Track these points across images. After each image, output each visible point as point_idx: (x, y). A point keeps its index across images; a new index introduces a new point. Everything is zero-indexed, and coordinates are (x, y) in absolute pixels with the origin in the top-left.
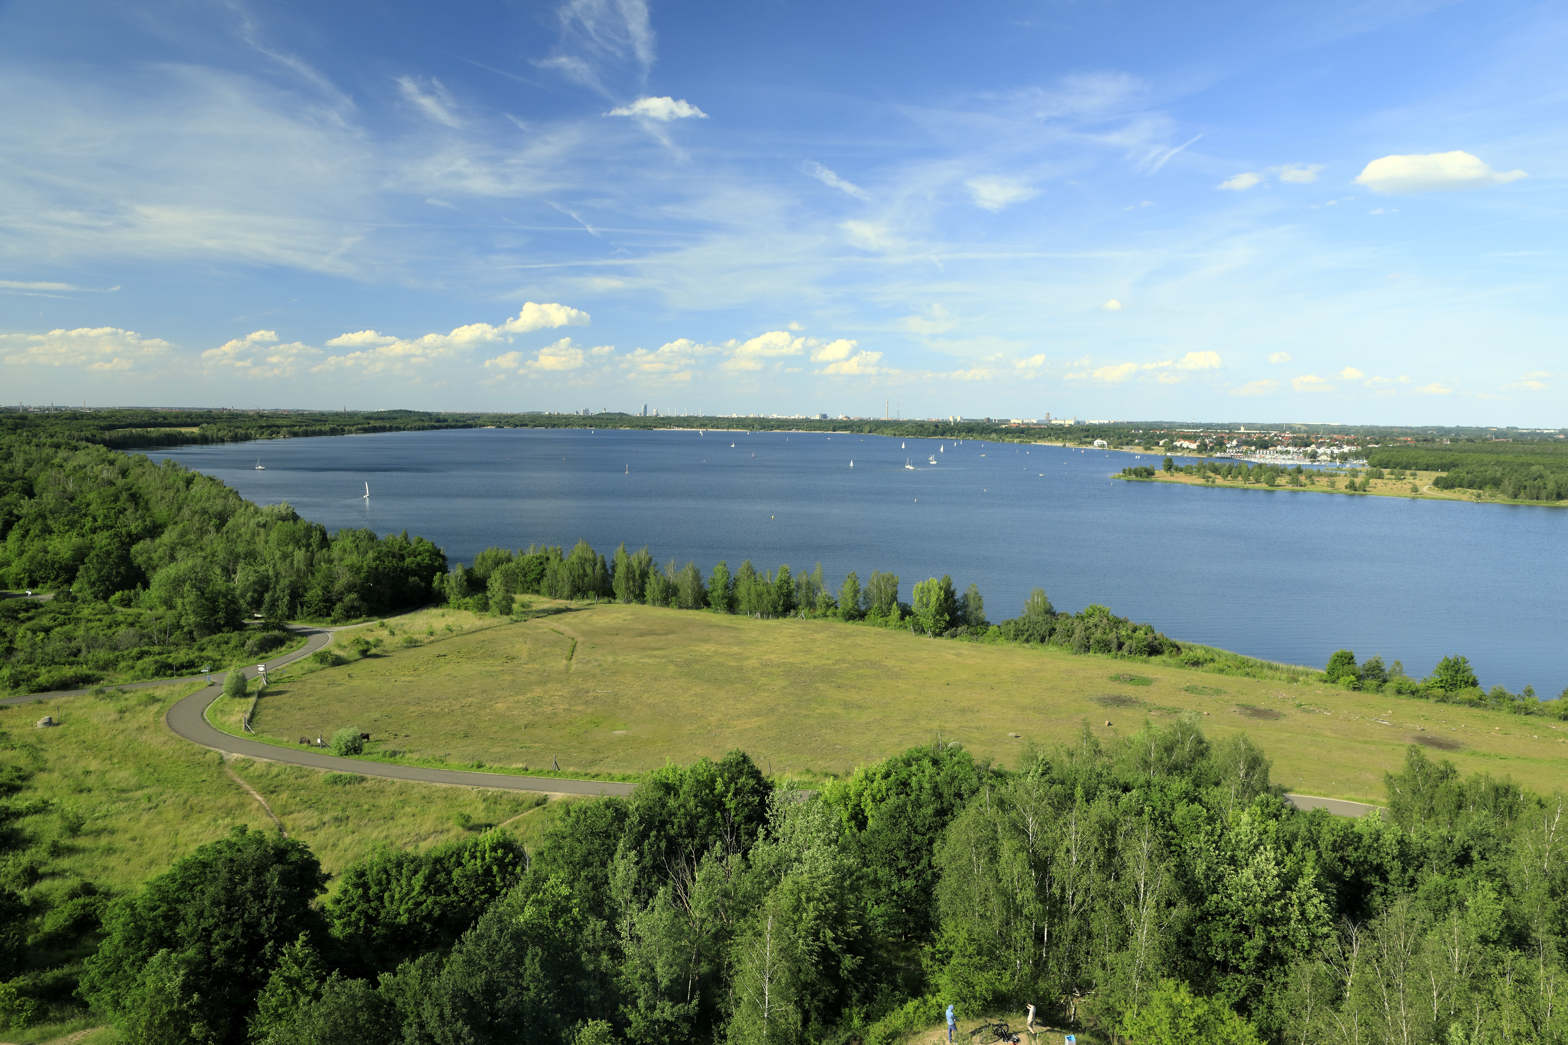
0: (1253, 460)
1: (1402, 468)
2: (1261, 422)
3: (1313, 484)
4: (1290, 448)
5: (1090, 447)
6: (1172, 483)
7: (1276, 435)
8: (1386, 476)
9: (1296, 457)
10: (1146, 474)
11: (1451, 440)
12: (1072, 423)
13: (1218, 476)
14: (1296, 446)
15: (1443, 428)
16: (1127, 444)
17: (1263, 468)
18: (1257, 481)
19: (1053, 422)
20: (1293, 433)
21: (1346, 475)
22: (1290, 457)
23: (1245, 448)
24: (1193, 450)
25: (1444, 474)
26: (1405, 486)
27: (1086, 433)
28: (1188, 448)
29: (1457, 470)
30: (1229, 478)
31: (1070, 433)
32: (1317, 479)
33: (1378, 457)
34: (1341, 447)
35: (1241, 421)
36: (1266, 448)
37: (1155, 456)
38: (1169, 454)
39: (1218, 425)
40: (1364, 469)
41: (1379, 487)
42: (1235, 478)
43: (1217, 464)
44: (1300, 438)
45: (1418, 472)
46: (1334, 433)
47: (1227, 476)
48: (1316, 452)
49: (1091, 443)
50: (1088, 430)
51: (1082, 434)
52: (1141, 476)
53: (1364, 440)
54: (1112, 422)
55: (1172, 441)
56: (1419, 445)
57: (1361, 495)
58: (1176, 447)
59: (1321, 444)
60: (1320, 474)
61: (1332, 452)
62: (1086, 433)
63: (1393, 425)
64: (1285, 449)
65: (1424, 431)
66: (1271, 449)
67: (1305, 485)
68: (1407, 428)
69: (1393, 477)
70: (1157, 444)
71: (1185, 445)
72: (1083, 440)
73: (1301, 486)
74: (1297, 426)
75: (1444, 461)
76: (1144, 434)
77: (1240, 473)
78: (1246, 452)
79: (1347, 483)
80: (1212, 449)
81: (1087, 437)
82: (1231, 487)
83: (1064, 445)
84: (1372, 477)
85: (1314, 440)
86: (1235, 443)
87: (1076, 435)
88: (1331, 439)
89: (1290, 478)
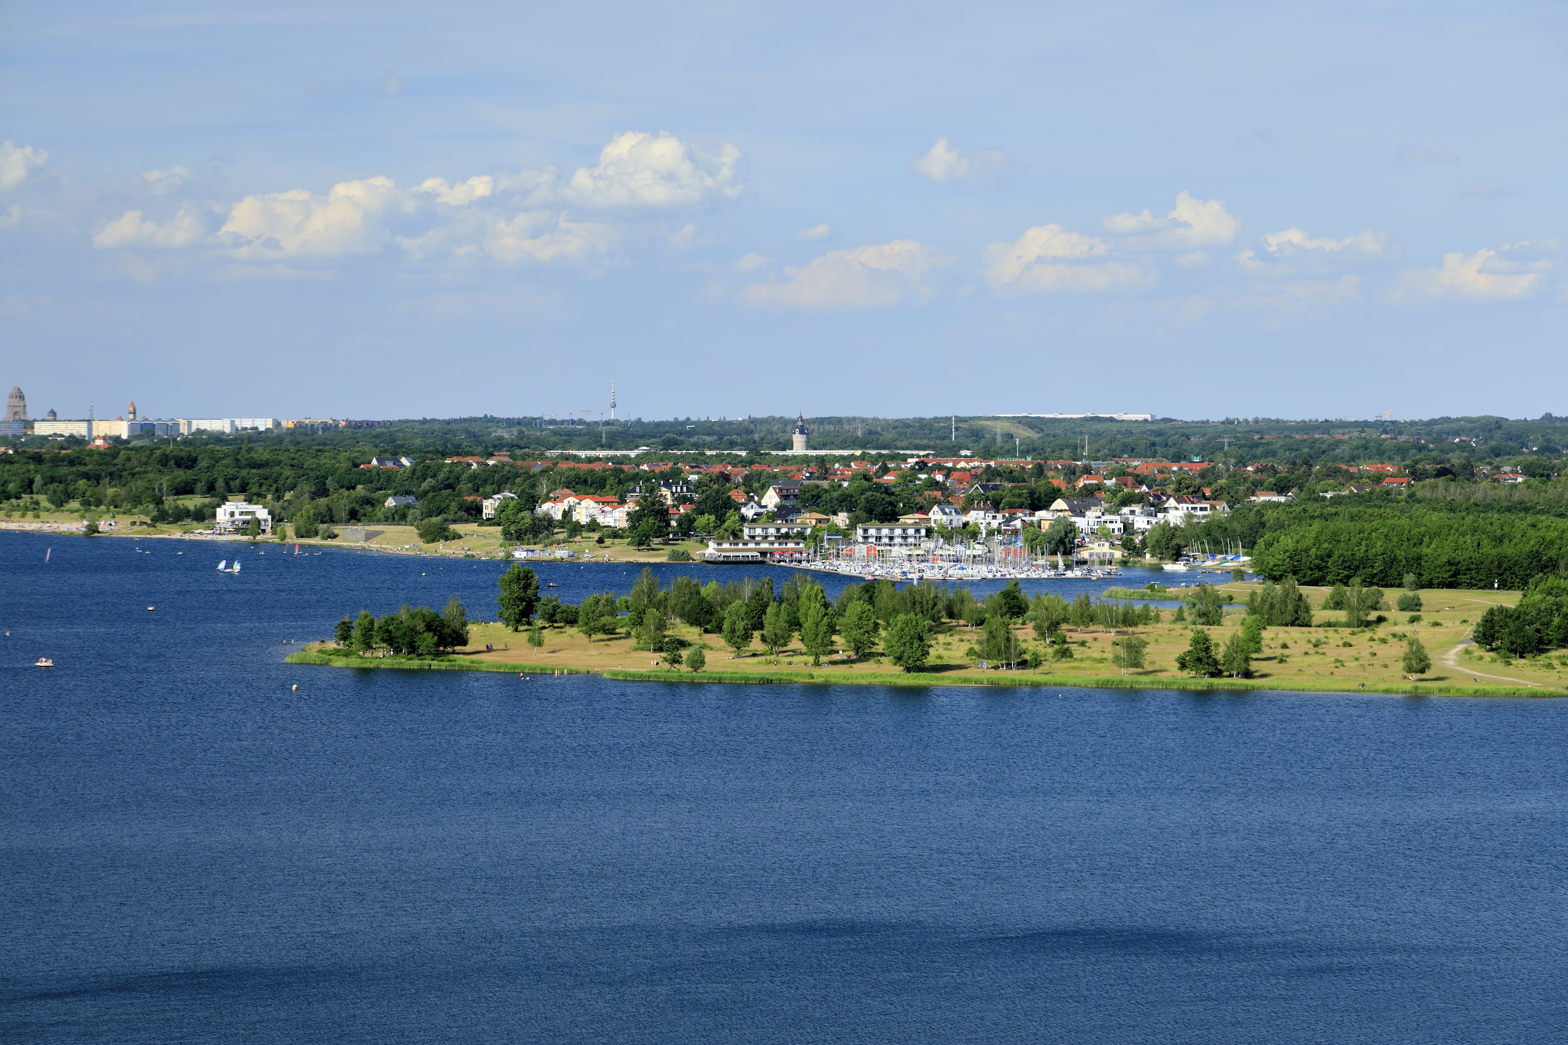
0: (844, 567)
1: (1368, 582)
2: (868, 413)
3: (1065, 654)
4: (976, 517)
5: (200, 533)
6: (539, 675)
7: (922, 466)
8: (1319, 615)
9: (999, 552)
10: (430, 638)
11: (1529, 471)
12: (122, 430)
13: (714, 639)
14: (996, 506)
15: (1498, 423)
16: (354, 516)
17: (884, 598)
18: (863, 654)
19: (42, 429)
20: (987, 454)
21: (1180, 618)
22: (979, 550)
23: (808, 520)
24: (616, 534)
25: (1510, 600)
26: (1383, 651)
27: (181, 475)
28: (593, 526)
29: (1552, 581)
30: (756, 644)
31: (115, 477)
32: (1077, 636)
33: (1287, 542)
34: (1158, 507)
35: (792, 414)
36: (890, 516)
37: (469, 565)
38: (520, 554)
39: (707, 428)
40: (1241, 590)
41: (1296, 660)
42: (777, 642)
43: (709, 590)
44: (1010, 476)
45: (1425, 595)
46: (1133, 452)
47: (747, 637)
48: (1071, 529)
49: (203, 516)
50: (189, 462)
51: (165, 481)
52: (413, 649)
53: (1237, 478)
54: (288, 424)
55: (531, 501)
56: (1421, 490)
57: (1238, 695)
58: (548, 523)
59: (1089, 495)
60: (1088, 618)
61: (1127, 527)
62: (181, 475)
63: (1333, 416)
64: (959, 520)
65: (1439, 438)
66: (908, 519)
67: (1037, 663)
68: (1381, 426)
69: (1341, 615)
70: (474, 512)
71: (581, 516)
72: (170, 502)
73: (1023, 664)
74: (1000, 428)
75: (1508, 549)
76: (420, 473)
77: (795, 624)
78: (815, 538)
79: (1186, 646)
80: (687, 529)
81: (186, 489)
82: (766, 683)
83: (93, 529)
84: (1270, 622)
85: (1059, 482)
86: (771, 499)
87: (139, 484)
88: (1121, 474)
89: (981, 634)
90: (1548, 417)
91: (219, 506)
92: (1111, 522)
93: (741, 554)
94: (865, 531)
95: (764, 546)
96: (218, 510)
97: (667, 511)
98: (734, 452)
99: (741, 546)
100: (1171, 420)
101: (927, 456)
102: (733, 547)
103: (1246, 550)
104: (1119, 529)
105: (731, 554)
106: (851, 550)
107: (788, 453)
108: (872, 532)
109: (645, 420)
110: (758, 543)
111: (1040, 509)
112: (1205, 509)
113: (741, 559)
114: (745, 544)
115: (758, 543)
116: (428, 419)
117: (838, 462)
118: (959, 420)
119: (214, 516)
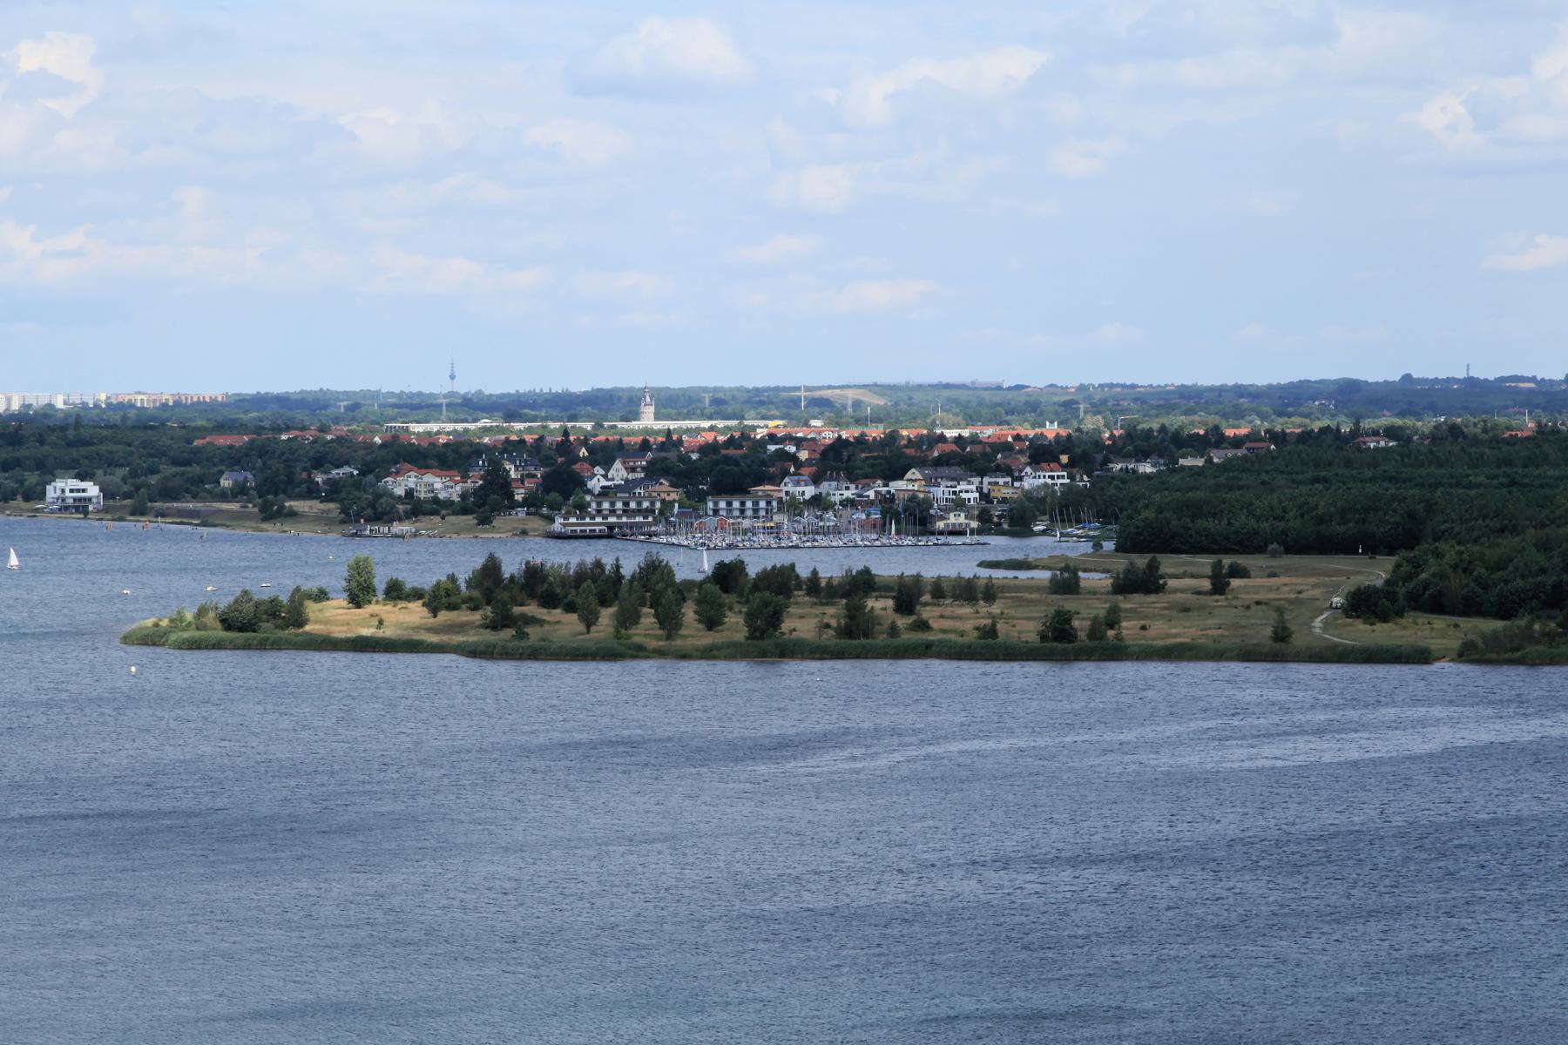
20: (838, 423)
91: (49, 483)
92: (967, 492)
94: (716, 504)
95: (612, 520)
97: (510, 483)
98: (578, 424)
99: (588, 520)
100: (1023, 387)
101: (777, 427)
103: (699, 405)
104: (975, 499)
108: (736, 504)
110: (605, 517)
112: (1063, 477)
114: (593, 518)
115: (605, 517)
119: (44, 493)
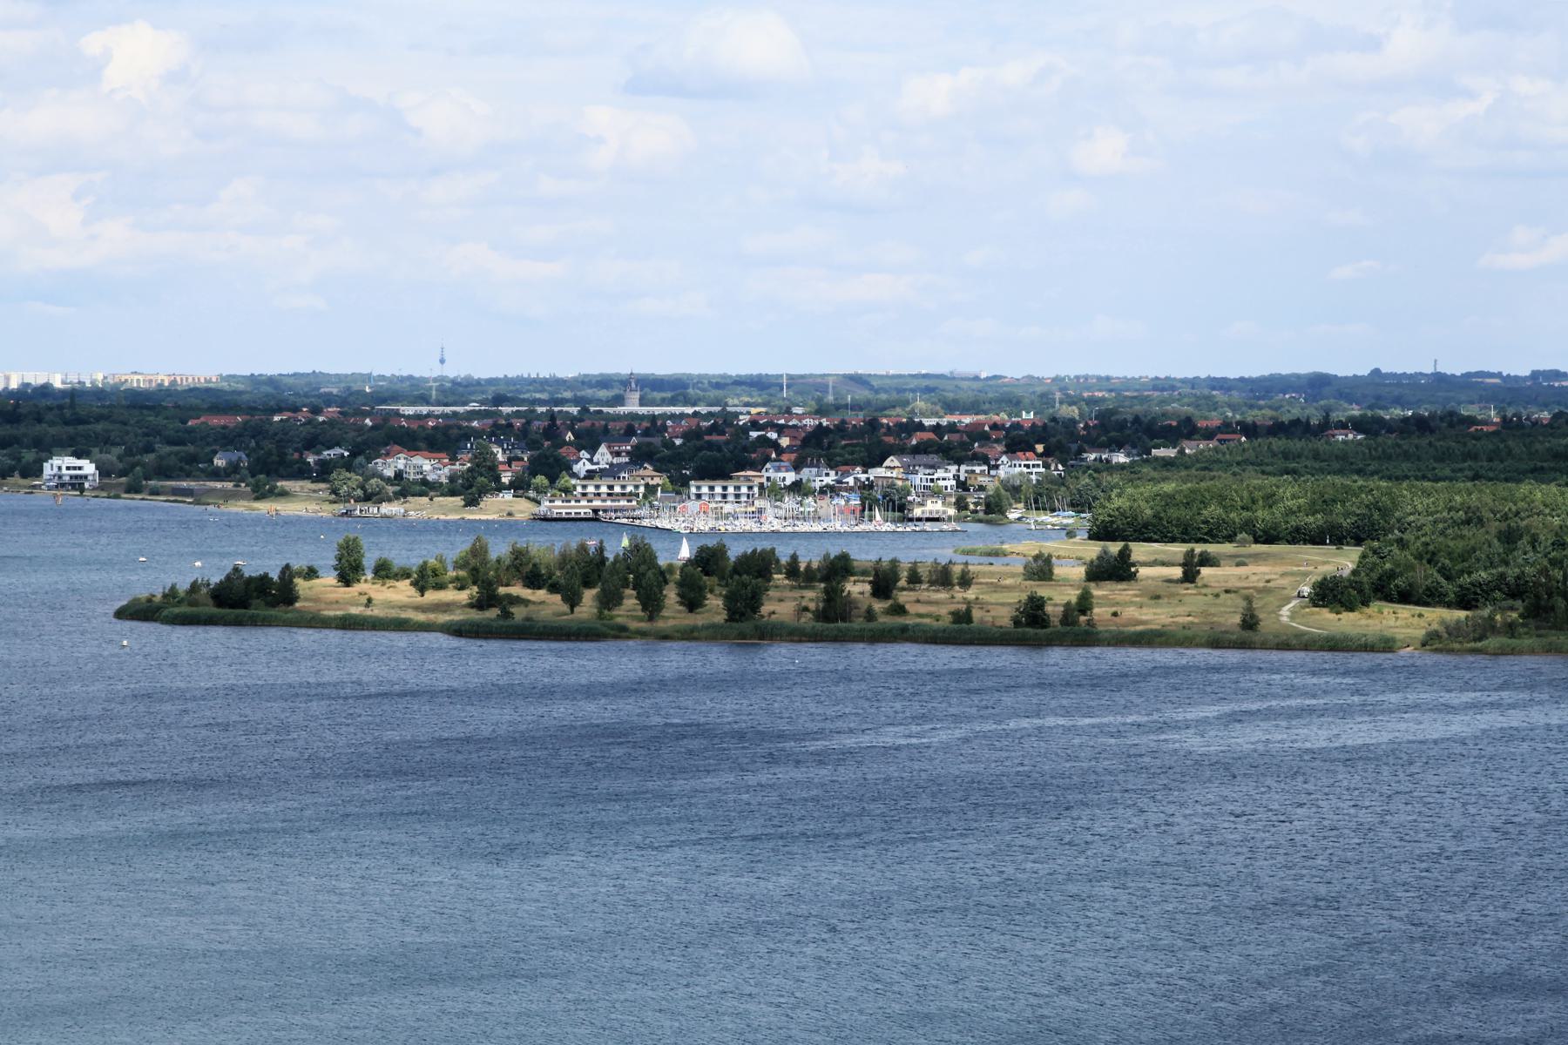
90: (1376, 372)
92: (944, 479)
93: (573, 511)
95: (597, 503)
96: (45, 464)
99: (573, 503)
100: (1001, 377)
102: (565, 504)
105: (564, 511)
106: (684, 507)
107: (621, 410)
109: (510, 376)
111: (874, 466)
112: (1038, 466)
113: (573, 516)
116: (1383, 371)
117: (670, 419)
118: (790, 377)
